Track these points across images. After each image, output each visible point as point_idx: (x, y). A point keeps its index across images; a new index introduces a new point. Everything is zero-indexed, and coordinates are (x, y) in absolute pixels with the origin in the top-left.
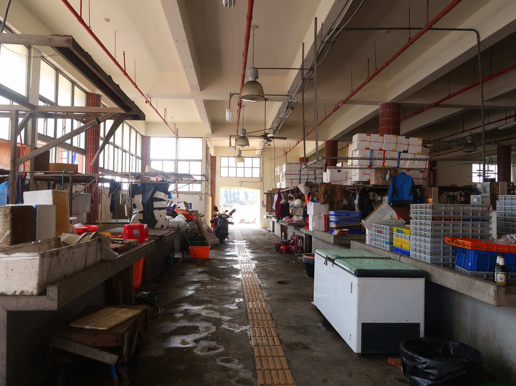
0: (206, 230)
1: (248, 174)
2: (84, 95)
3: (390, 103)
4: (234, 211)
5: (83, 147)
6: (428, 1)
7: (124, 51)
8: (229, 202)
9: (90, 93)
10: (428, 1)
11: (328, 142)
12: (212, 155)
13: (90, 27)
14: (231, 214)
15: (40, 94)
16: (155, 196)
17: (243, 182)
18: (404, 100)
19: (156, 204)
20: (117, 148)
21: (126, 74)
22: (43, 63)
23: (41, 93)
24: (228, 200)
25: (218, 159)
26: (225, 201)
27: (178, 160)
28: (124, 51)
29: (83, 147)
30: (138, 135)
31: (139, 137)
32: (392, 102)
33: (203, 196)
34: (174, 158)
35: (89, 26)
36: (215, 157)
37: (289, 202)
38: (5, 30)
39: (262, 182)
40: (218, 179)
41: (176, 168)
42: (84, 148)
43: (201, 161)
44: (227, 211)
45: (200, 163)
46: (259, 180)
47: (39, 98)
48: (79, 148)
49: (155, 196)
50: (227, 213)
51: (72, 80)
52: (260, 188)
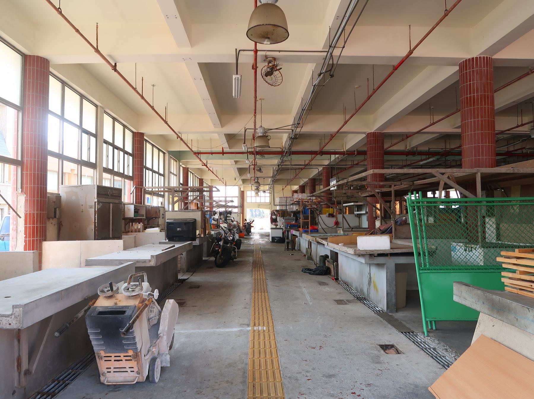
0: (242, 229)
1: (263, 201)
2: (18, 59)
3: (480, 57)
4: (253, 221)
5: (131, 175)
6: (445, 1)
7: (97, 23)
8: (254, 216)
9: (185, 167)
10: (445, 1)
11: (300, 186)
12: (242, 190)
13: (136, 88)
14: (252, 222)
15: (104, 138)
16: (227, 216)
17: (260, 205)
18: (317, 177)
19: (228, 218)
20: (155, 173)
21: (213, 173)
22: (105, 116)
23: (104, 138)
24: (253, 214)
25: (245, 192)
26: (250, 215)
27: (227, 197)
28: (142, 77)
29: (131, 175)
30: (198, 179)
31: (198, 179)
32: (379, 132)
33: (239, 214)
34: (225, 196)
35: (152, 106)
36: (244, 191)
37: (433, 195)
38: (84, 99)
39: (271, 205)
40: (245, 204)
41: (432, 325)
42: (132, 176)
43: (238, 197)
44: (251, 221)
45: (237, 198)
46: (269, 204)
47: (104, 141)
48: (89, 162)
49: (227, 216)
50: (251, 222)
51: (132, 131)
52: (269, 208)
